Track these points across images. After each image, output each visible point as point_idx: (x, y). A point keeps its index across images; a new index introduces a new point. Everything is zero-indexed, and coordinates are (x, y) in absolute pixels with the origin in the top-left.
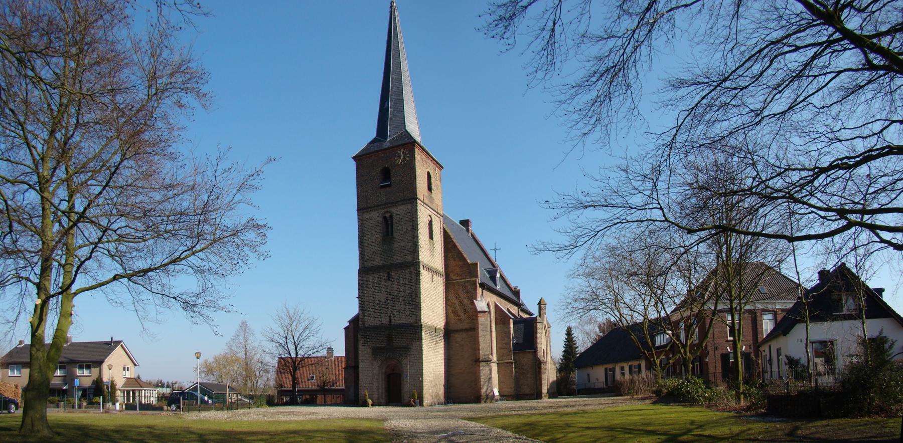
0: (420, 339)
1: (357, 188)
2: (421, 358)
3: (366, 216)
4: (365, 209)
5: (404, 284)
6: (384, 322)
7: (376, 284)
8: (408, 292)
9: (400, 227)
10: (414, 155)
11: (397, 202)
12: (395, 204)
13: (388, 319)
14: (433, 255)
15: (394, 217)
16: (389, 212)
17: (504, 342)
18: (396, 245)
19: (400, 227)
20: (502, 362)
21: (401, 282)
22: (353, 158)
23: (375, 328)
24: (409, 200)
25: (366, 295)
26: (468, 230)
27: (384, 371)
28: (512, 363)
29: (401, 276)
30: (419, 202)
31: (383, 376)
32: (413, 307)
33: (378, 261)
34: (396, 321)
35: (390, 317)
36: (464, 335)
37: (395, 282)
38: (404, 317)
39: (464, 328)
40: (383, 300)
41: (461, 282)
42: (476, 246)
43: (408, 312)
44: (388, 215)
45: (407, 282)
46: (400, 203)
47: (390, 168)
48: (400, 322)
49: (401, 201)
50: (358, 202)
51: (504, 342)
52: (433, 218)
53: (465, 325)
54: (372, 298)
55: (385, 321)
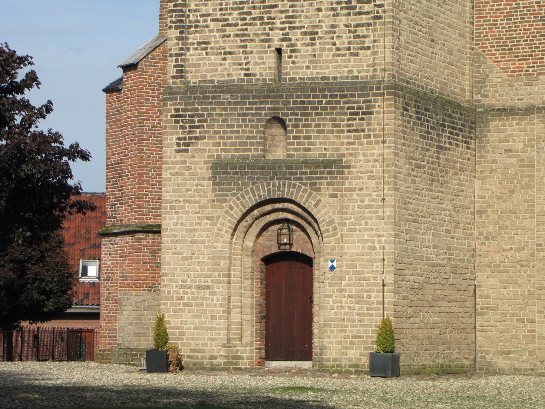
35: (279, 51)
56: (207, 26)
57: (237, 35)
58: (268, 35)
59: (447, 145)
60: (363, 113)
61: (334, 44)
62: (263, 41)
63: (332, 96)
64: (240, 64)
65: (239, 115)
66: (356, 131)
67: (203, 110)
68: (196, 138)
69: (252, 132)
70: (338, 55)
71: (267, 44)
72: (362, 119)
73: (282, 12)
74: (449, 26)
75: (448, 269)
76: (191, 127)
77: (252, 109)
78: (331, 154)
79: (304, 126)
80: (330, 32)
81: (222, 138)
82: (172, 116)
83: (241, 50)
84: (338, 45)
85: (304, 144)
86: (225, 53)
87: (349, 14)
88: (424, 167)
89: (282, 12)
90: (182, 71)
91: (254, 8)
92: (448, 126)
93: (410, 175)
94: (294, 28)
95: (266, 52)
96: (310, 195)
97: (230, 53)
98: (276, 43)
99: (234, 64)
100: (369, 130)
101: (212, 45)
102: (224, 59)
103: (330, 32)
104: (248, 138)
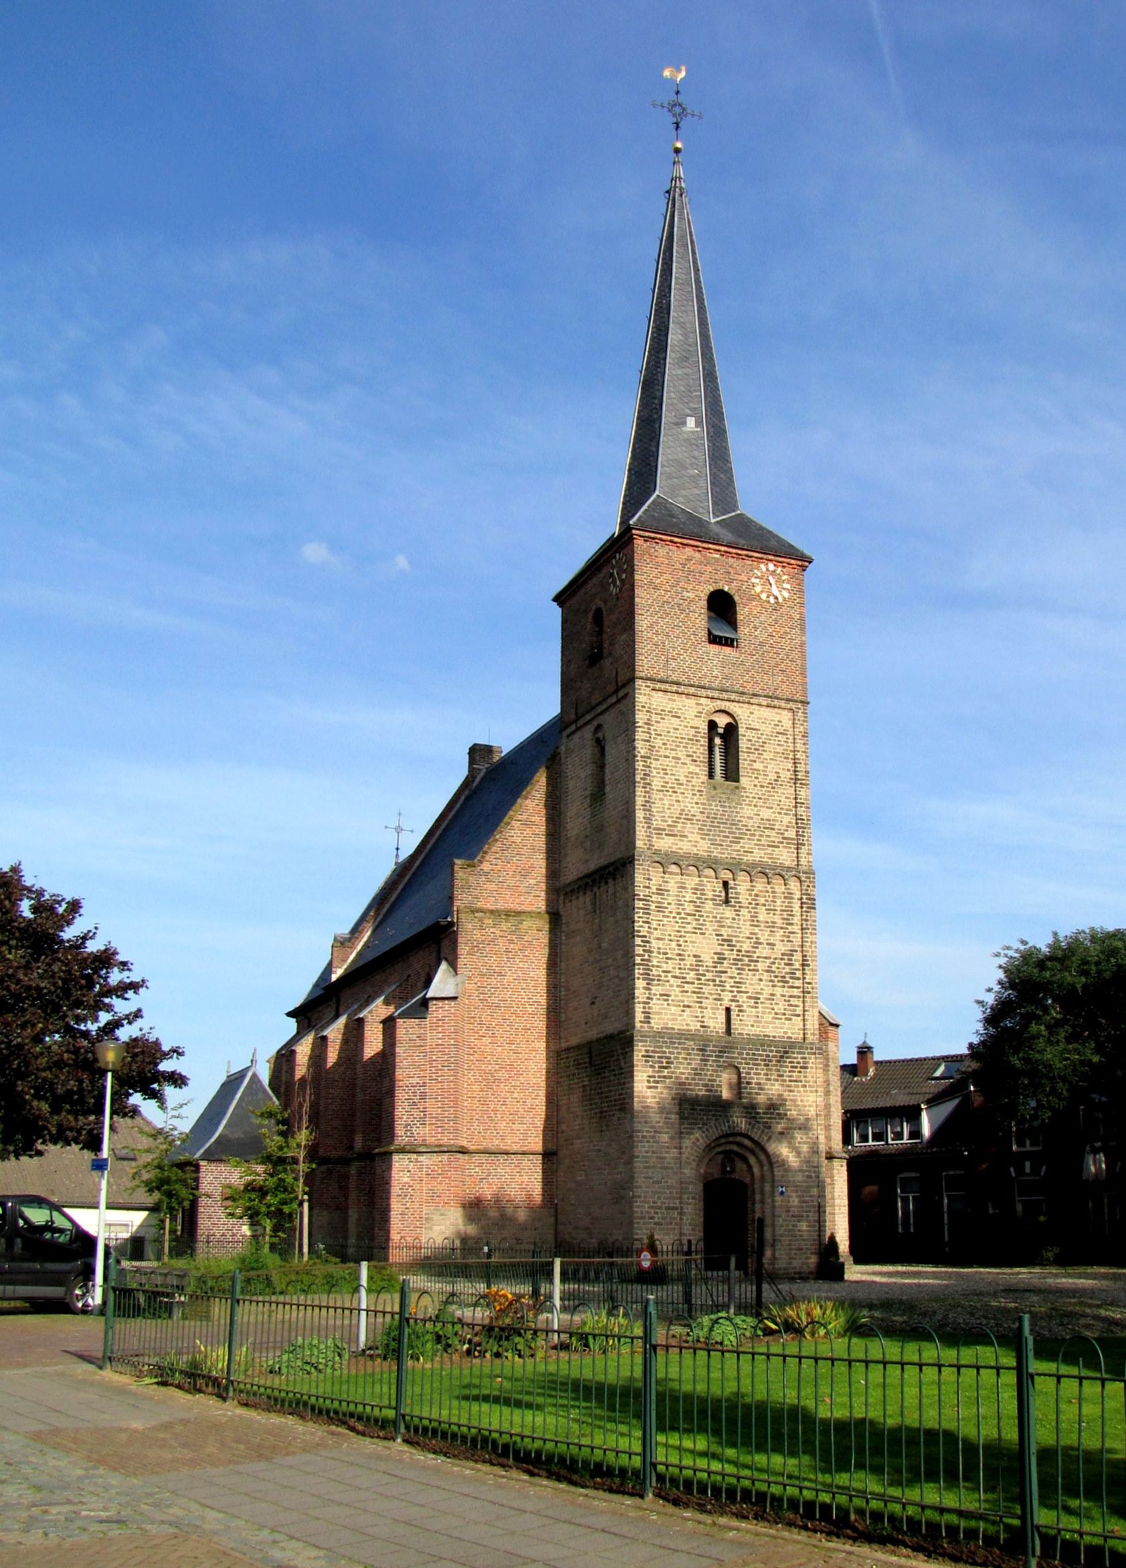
8: (781, 948)
37: (744, 912)
54: (674, 944)
56: (668, 981)
57: (694, 992)
58: (720, 995)
60: (801, 1067)
61: (773, 1009)
62: (715, 999)
64: (697, 1017)
66: (796, 1081)
70: (777, 1018)
71: (719, 1003)
72: (800, 1072)
73: (731, 978)
76: (659, 1067)
79: (755, 1074)
80: (769, 999)
82: (643, 1056)
83: (698, 1005)
86: (684, 1006)
87: (784, 987)
90: (649, 1018)
91: (708, 971)
94: (741, 992)
95: (718, 1009)
96: (763, 1132)
97: (689, 1007)
98: (726, 1003)
99: (692, 1016)
100: (806, 1081)
101: (673, 998)
102: (683, 1011)
103: (769, 999)
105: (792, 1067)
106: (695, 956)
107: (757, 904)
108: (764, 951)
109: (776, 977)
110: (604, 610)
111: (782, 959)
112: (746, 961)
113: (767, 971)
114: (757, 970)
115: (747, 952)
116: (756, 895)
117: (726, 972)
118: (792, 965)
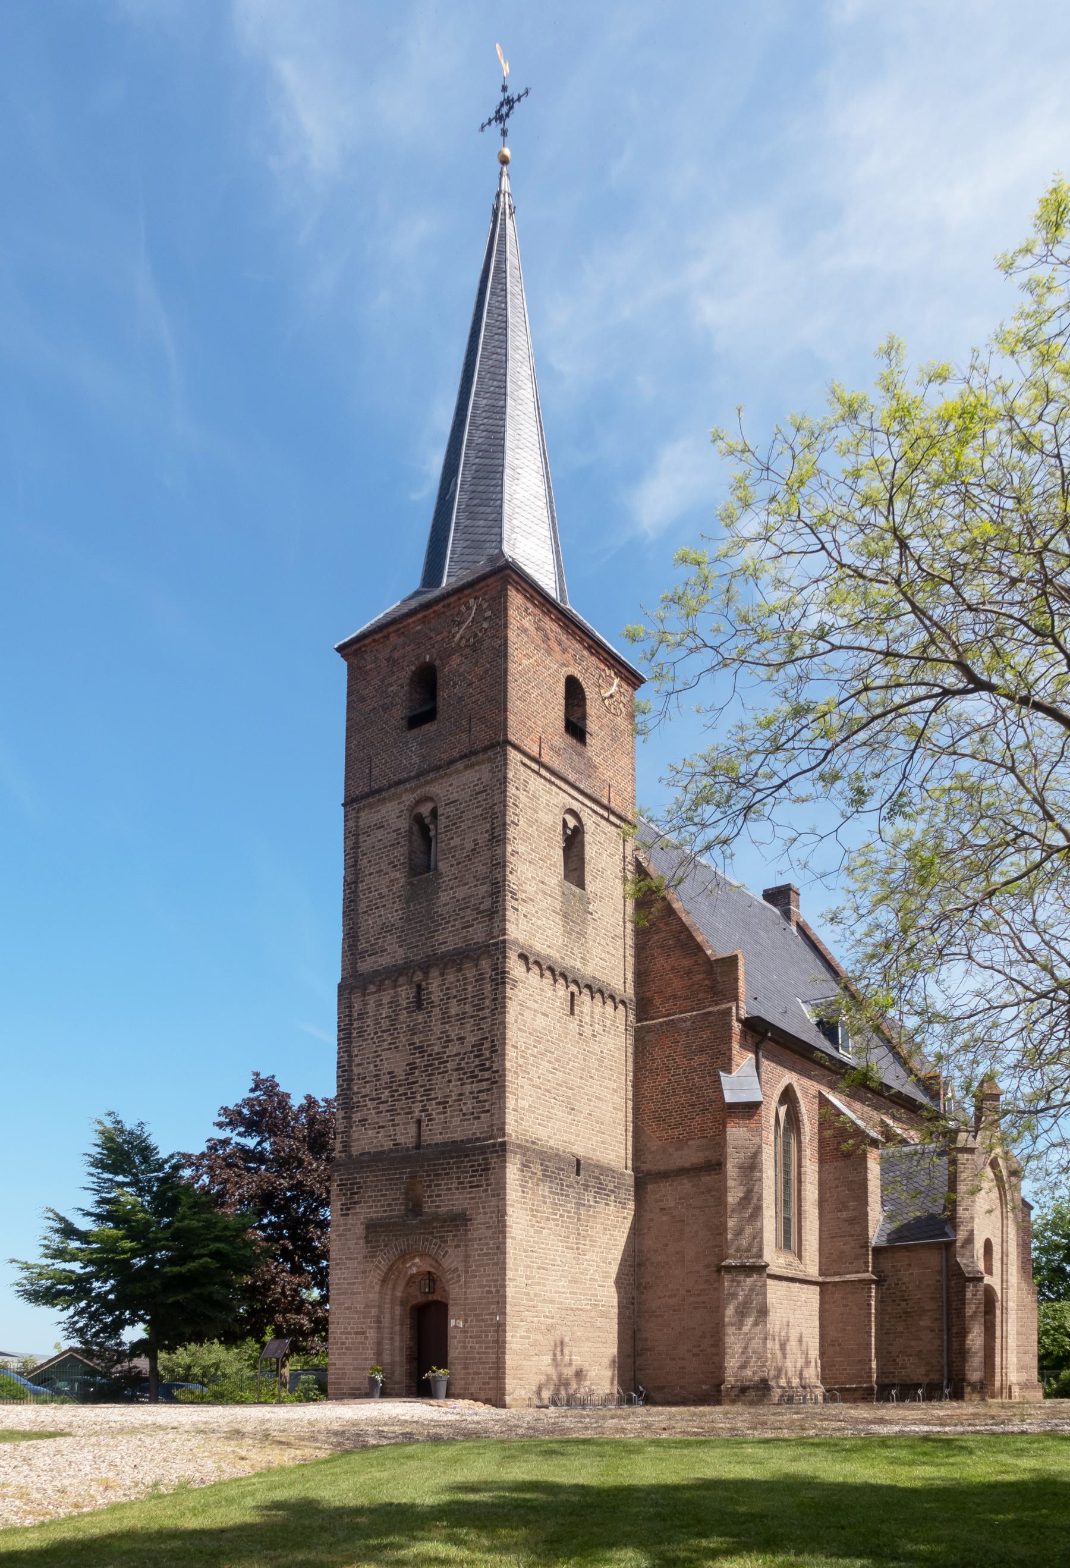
0: (499, 1191)
1: (348, 738)
2: (500, 1249)
3: (368, 818)
4: (366, 796)
5: (462, 1018)
6: (401, 1139)
7: (385, 1024)
8: (471, 1040)
9: (456, 841)
10: (506, 609)
11: (451, 762)
12: (439, 768)
13: (412, 1130)
14: (582, 934)
15: (440, 811)
16: (430, 799)
17: (844, 1215)
18: (444, 897)
19: (456, 841)
20: (837, 1279)
21: (453, 1011)
22: (340, 649)
23: (376, 1159)
24: (485, 749)
25: (357, 1060)
26: (787, 915)
27: (399, 1294)
28: (868, 1282)
29: (454, 992)
30: (513, 754)
31: (398, 1310)
32: (485, 1085)
33: (394, 954)
34: (435, 1135)
35: (419, 1122)
36: (686, 1186)
37: (436, 1011)
38: (456, 1121)
39: (687, 1165)
40: (400, 1072)
41: (684, 1020)
42: (810, 956)
43: (469, 1105)
44: (425, 810)
45: (468, 1008)
46: (460, 765)
47: (437, 663)
48: (446, 1137)
49: (462, 758)
50: (347, 779)
51: (844, 1215)
52: (584, 820)
53: (691, 1156)
55: (406, 1136)
57: (388, 1111)
59: (592, 1203)
60: (482, 1170)
61: (461, 1110)
63: (457, 1157)
65: (387, 1180)
67: (361, 1178)
68: (355, 1203)
69: (395, 1194)
70: (464, 1120)
74: (597, 1098)
75: (593, 1314)
77: (395, 1174)
78: (457, 1209)
81: (374, 1201)
84: (464, 1111)
85: (435, 1201)
87: (472, 1082)
88: (557, 1220)
89: (421, 1086)
91: (400, 1085)
92: (594, 1187)
93: (532, 1226)
97: (383, 1127)
104: (393, 1200)
105: (473, 1171)
106: (389, 1073)
107: (449, 998)
108: (454, 1048)
109: (465, 1073)
110: (578, 676)
111: (472, 1052)
112: (434, 1064)
113: (456, 1070)
114: (447, 1072)
115: (438, 1054)
116: (448, 989)
117: (417, 1082)
118: (482, 1055)
